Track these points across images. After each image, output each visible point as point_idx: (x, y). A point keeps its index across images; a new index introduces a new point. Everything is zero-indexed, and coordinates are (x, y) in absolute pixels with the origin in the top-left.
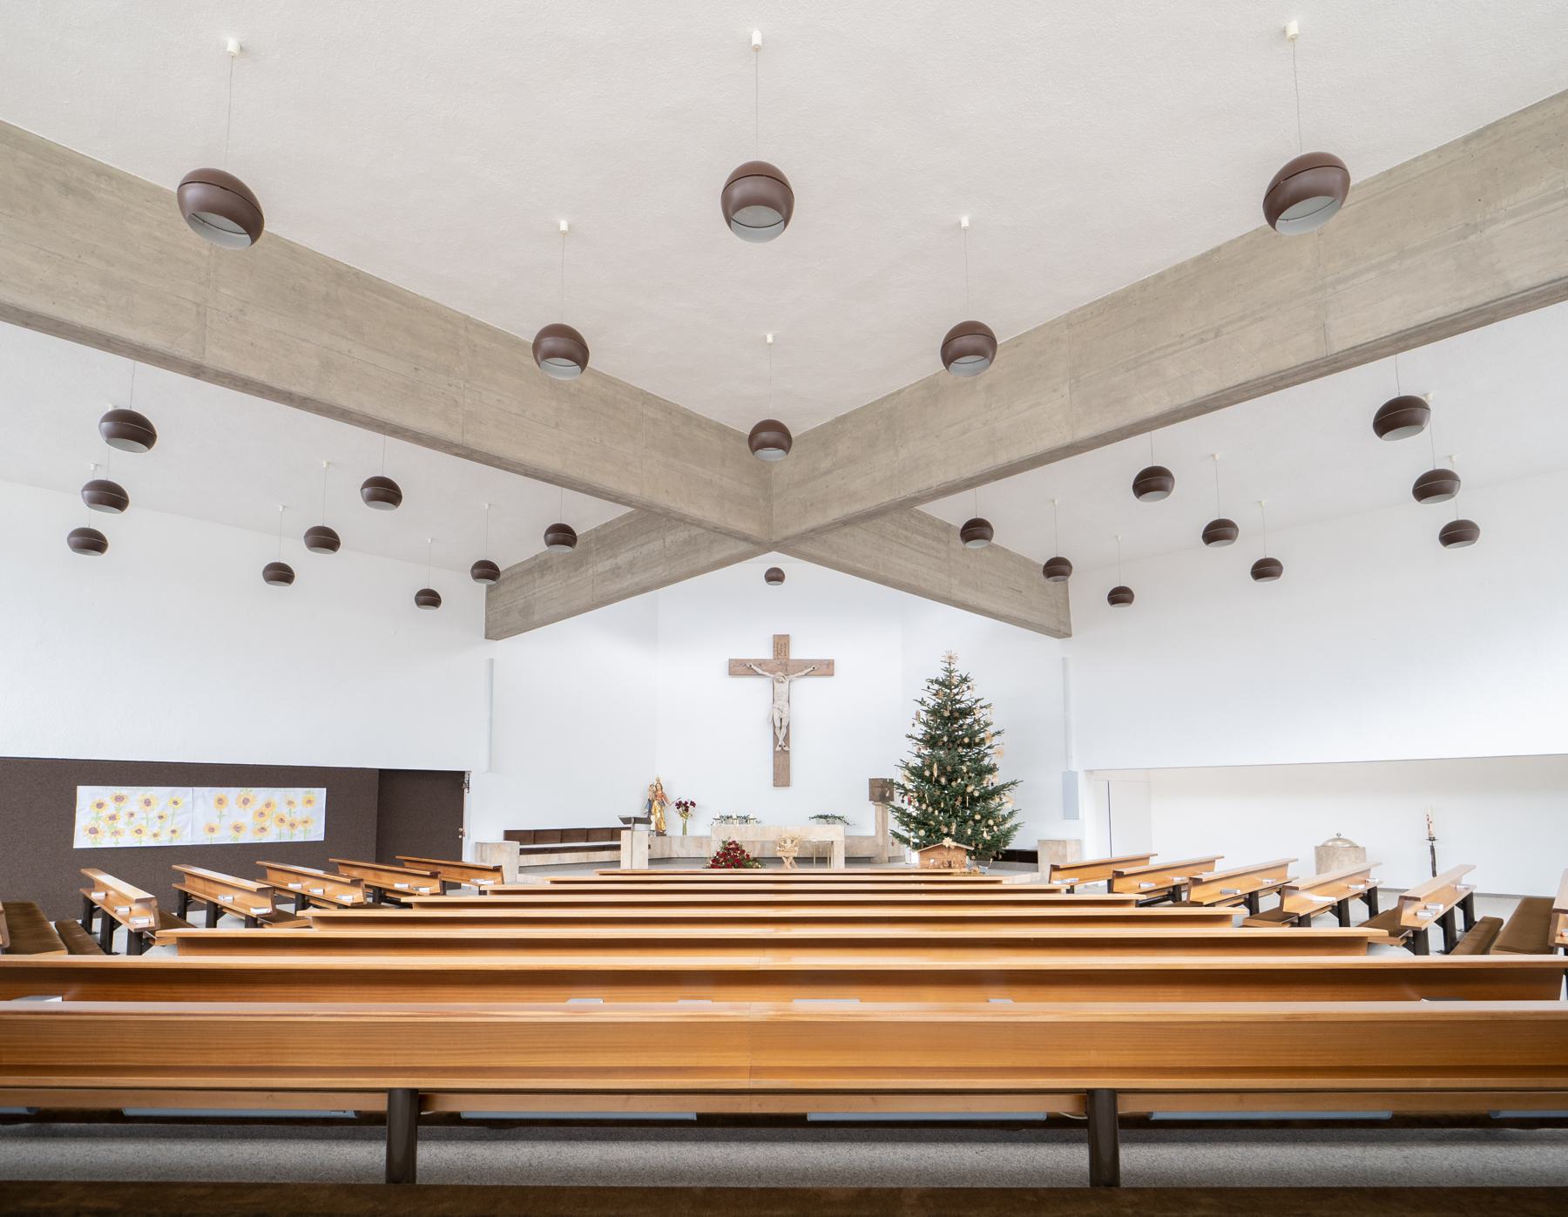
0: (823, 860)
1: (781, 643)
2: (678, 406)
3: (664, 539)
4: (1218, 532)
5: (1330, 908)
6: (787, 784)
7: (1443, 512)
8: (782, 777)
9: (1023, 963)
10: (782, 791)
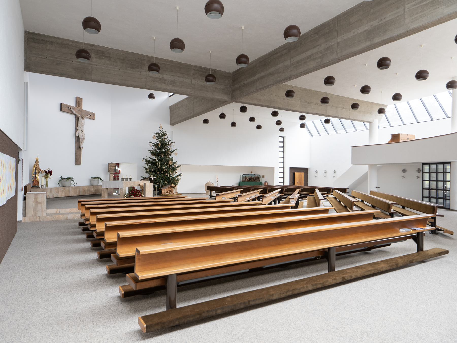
0: (99, 195)
1: (79, 101)
2: (264, 55)
3: (326, 111)
4: (252, 119)
5: (252, 200)
6: (279, 178)
7: (279, 127)
8: (78, 161)
9: (268, 221)
10: (77, 166)
